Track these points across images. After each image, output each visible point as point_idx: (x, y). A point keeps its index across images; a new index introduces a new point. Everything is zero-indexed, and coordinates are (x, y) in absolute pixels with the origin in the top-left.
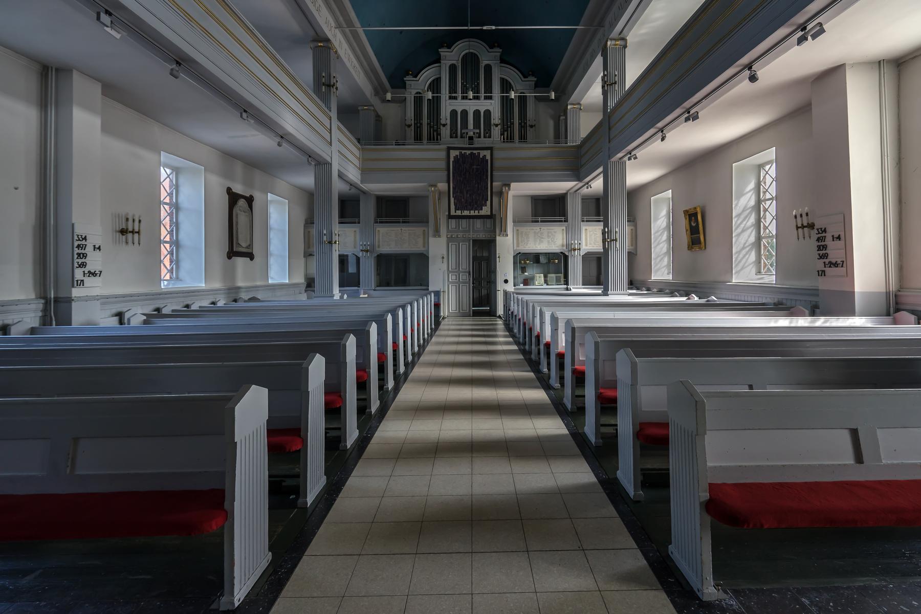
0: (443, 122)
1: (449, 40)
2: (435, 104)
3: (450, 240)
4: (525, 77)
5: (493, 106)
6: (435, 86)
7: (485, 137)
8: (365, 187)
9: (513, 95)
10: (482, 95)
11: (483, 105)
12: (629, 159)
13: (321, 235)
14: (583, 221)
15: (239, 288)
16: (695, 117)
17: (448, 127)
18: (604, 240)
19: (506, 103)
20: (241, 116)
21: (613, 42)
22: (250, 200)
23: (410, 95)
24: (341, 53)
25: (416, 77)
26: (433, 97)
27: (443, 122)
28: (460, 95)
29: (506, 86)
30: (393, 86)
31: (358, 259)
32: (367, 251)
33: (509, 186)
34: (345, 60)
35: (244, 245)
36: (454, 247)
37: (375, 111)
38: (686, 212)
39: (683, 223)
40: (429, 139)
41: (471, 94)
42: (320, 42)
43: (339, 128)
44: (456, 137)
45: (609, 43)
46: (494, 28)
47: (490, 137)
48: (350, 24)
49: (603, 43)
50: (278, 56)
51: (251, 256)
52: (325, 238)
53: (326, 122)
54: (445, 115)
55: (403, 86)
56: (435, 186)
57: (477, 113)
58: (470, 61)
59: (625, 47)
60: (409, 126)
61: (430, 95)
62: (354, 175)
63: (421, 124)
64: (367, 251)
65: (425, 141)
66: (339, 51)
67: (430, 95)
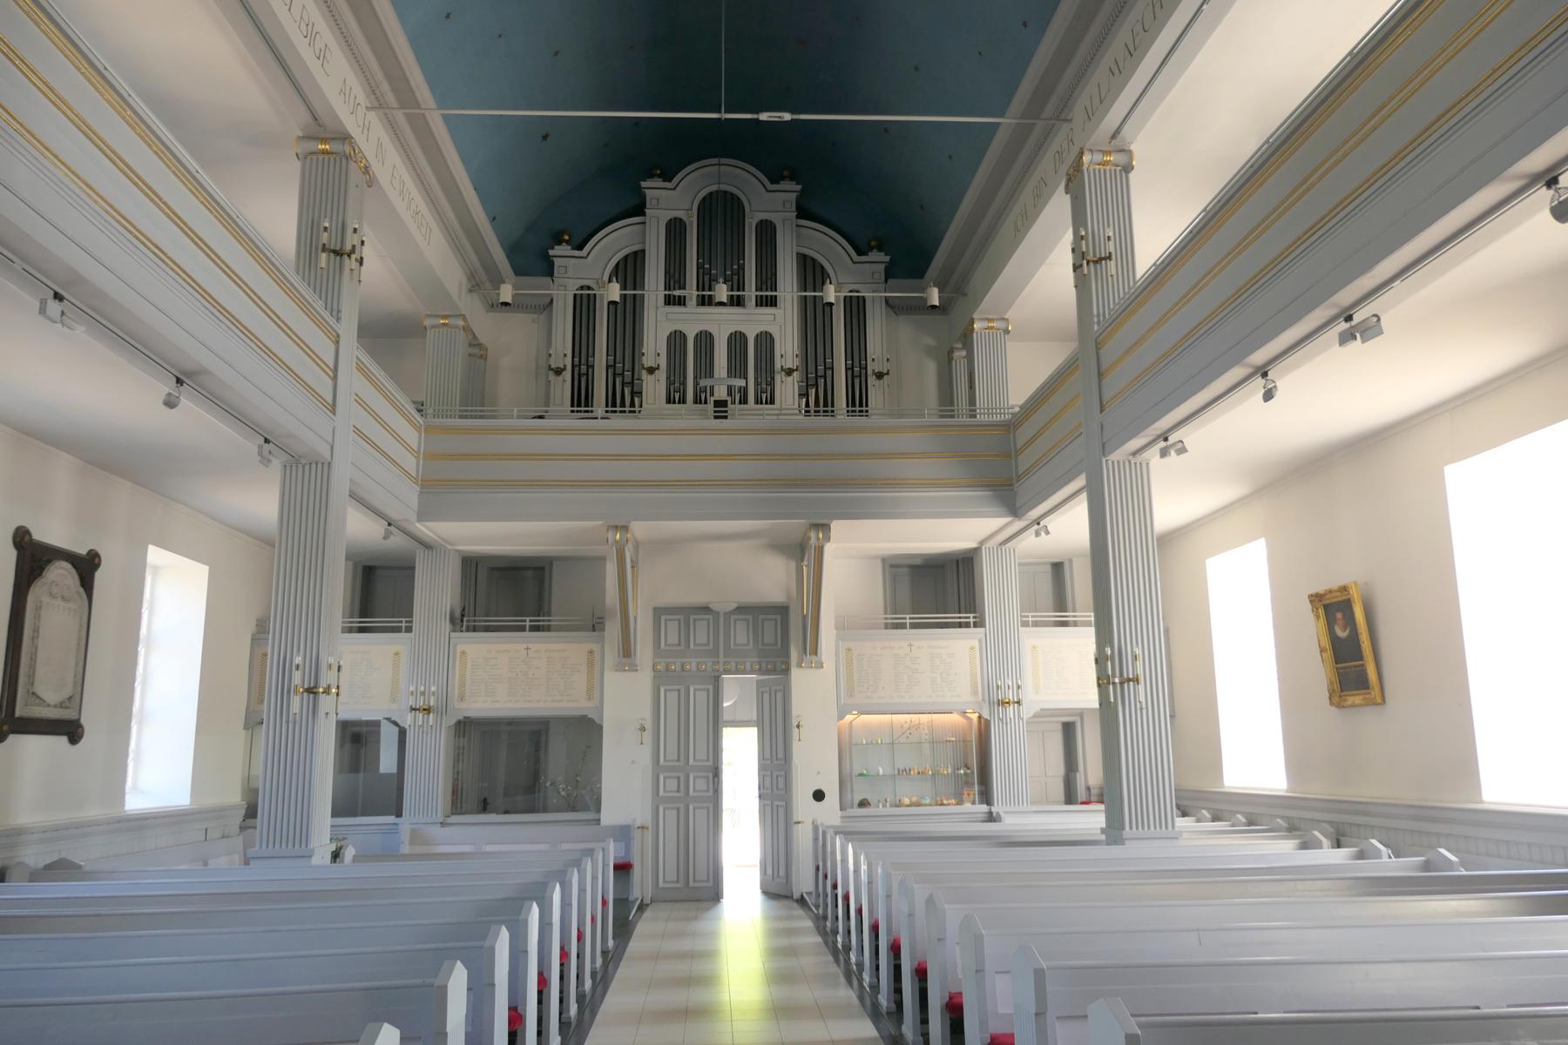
0: (648, 361)
1: (669, 152)
2: (628, 315)
3: (662, 678)
4: (860, 252)
5: (781, 324)
6: (630, 269)
7: (758, 401)
8: (426, 530)
9: (831, 294)
10: (751, 293)
11: (751, 321)
12: (1164, 453)
13: (285, 668)
14: (1025, 624)
15: (19, 832)
16: (1370, 330)
17: (662, 375)
18: (1103, 682)
19: (814, 317)
20: (42, 311)
21: (1098, 157)
22: (86, 567)
23: (563, 294)
24: (381, 172)
25: (580, 247)
26: (624, 297)
27: (648, 361)
28: (691, 292)
29: (812, 273)
30: (519, 271)
31: (402, 733)
32: (428, 710)
33: (825, 528)
34: (392, 194)
35: (51, 697)
36: (673, 697)
37: (467, 329)
38: (1316, 599)
39: (1311, 629)
40: (612, 402)
41: (722, 292)
42: (324, 140)
43: (361, 368)
44: (683, 401)
45: (1086, 158)
46: (787, 117)
47: (772, 402)
48: (407, 99)
49: (1070, 159)
50: (204, 176)
51: (72, 731)
52: (297, 678)
53: (326, 350)
54: (654, 347)
55: (549, 270)
56: (625, 528)
57: (737, 341)
58: (721, 212)
59: (1128, 168)
60: (559, 372)
61: (614, 292)
62: (404, 500)
63: (591, 367)
64: (428, 710)
65: (599, 408)
66: (375, 167)
67: (614, 292)
